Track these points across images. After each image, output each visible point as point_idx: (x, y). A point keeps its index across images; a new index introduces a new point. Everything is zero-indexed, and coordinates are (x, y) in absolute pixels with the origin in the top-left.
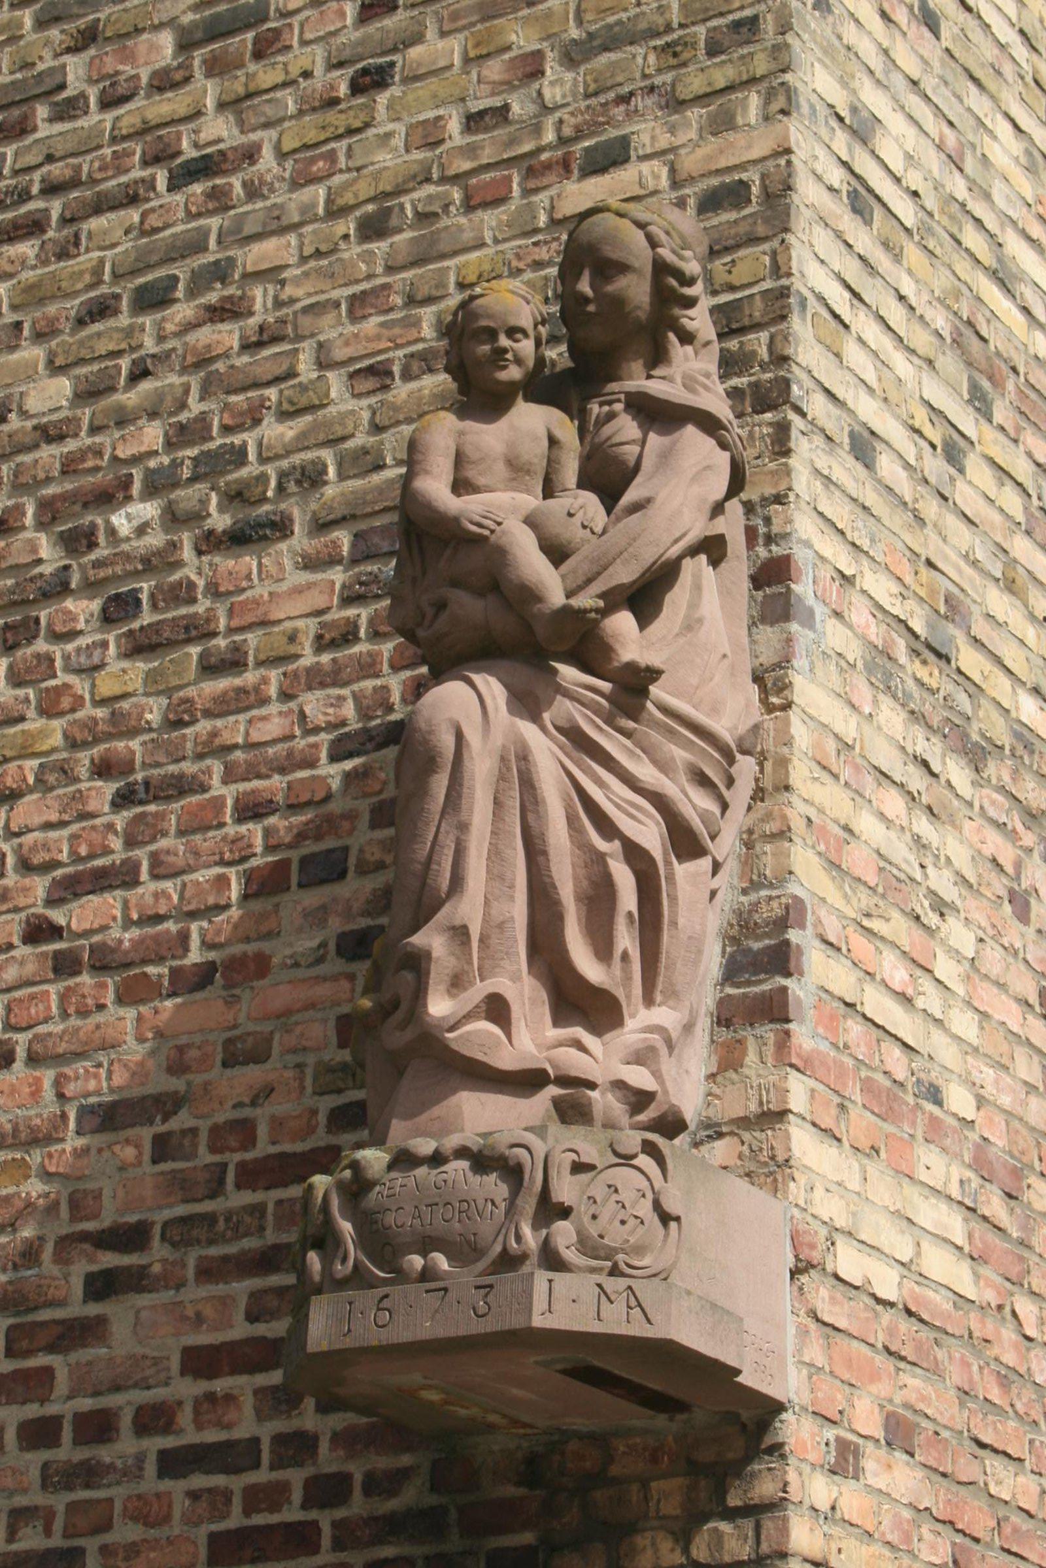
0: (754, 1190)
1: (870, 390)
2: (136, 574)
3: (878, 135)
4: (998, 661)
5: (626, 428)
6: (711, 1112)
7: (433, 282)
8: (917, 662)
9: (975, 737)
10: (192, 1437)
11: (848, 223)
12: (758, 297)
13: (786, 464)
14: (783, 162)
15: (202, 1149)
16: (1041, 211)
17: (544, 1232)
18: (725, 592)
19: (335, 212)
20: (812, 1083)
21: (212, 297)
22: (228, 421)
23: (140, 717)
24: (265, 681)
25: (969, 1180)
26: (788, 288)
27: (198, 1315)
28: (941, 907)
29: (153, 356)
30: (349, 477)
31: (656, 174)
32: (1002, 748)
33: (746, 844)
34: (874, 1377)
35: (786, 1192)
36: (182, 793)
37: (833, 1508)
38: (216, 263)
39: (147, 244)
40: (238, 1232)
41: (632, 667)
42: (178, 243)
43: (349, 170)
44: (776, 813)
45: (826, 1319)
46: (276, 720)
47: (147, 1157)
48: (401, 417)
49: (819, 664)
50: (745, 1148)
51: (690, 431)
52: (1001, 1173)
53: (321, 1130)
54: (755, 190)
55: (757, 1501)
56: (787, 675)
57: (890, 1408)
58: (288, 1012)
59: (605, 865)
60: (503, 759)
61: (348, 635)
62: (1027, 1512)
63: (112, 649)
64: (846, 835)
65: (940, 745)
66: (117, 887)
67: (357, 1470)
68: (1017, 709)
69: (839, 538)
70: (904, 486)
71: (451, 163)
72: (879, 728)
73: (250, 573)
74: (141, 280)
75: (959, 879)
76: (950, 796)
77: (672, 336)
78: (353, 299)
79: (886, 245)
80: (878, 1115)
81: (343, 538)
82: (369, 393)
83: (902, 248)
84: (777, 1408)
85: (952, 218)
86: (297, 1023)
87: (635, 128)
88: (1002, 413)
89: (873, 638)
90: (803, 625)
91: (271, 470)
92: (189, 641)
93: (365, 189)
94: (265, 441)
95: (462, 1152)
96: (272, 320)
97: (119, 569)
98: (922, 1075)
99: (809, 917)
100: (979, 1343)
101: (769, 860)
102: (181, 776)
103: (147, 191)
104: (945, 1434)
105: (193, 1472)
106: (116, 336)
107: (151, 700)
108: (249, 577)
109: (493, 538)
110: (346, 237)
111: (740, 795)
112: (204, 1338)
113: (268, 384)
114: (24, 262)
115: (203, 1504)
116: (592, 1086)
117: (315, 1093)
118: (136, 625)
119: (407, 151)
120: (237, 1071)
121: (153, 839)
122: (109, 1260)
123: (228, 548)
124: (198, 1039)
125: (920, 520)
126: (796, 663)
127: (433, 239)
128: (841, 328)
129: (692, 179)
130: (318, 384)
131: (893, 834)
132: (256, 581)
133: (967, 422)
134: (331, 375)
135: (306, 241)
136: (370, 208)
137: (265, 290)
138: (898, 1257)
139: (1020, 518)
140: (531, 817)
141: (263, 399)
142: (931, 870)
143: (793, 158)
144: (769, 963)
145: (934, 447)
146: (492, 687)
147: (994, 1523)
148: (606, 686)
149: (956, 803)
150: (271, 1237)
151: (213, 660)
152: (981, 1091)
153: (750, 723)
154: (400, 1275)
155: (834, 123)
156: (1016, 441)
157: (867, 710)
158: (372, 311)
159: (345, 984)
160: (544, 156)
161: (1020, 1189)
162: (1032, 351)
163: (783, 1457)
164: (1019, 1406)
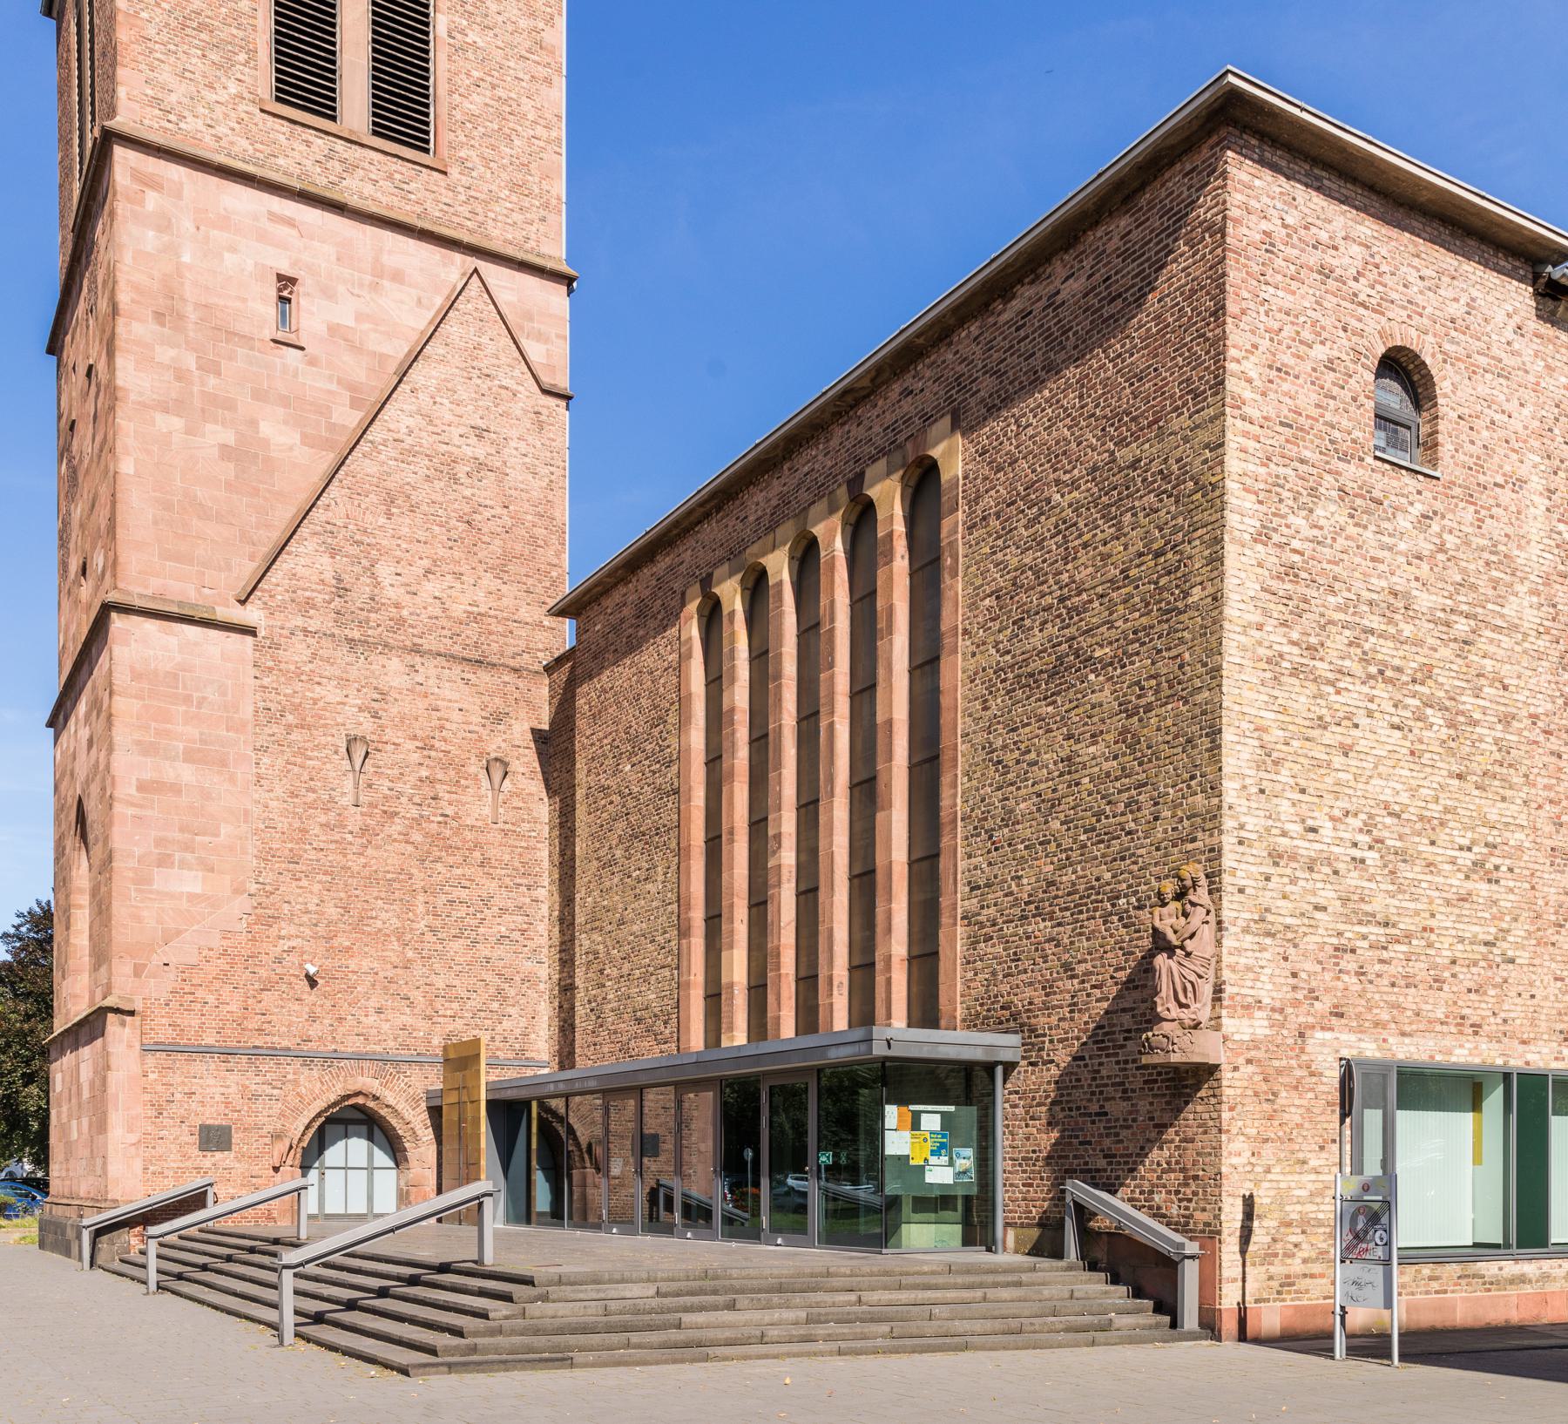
5: (1188, 906)
114: (1214, 733)
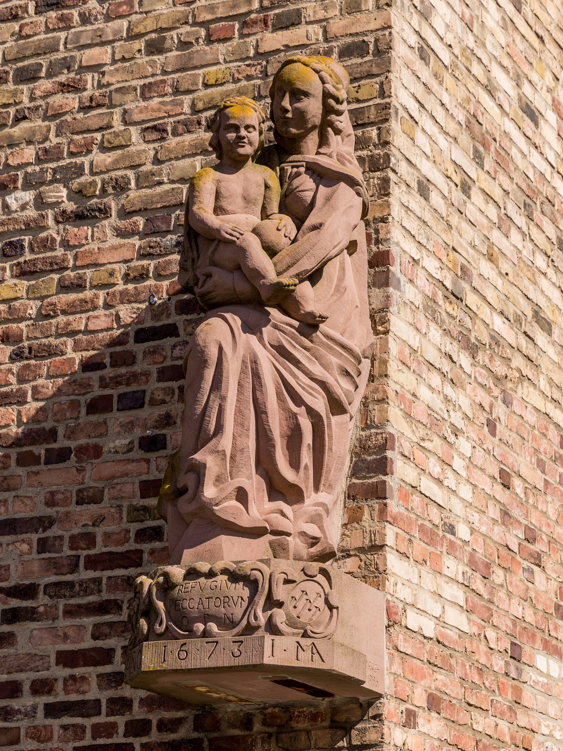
0: (366, 586)
1: (428, 157)
2: (21, 232)
3: (433, 15)
4: (484, 298)
6: (344, 543)
7: (190, 82)
8: (447, 304)
9: (473, 340)
10: (62, 697)
11: (418, 65)
12: (373, 107)
13: (387, 201)
14: (387, 33)
15: (66, 548)
16: (509, 50)
17: (269, 612)
18: (356, 271)
19: (132, 36)
20: (397, 530)
21: (62, 78)
22: (73, 149)
23: (25, 311)
24: (96, 296)
25: (467, 572)
26: (389, 104)
27: (65, 634)
28: (456, 432)
29: (29, 108)
30: (143, 188)
31: (316, 31)
32: (485, 345)
33: (364, 404)
34: (423, 677)
35: (384, 586)
36: (50, 355)
37: (404, 744)
38: (65, 58)
39: (24, 44)
40: (86, 592)
41: (311, 315)
42: (42, 45)
43: (141, 13)
44: (380, 389)
45: (402, 650)
46: (103, 319)
47: (35, 549)
48: (173, 156)
49: (402, 309)
50: (363, 563)
51: (342, 185)
52: (481, 566)
53: (132, 540)
54: (371, 47)
55: (368, 743)
56: (387, 315)
57: (430, 691)
58: (113, 477)
59: (297, 418)
60: (243, 362)
61: (143, 276)
62: (490, 736)
63: (8, 273)
64: (413, 399)
65: (457, 346)
66: (15, 404)
67: (154, 718)
68: (493, 324)
69: (413, 239)
70: (443, 209)
71: (200, 14)
72: (429, 340)
73: (87, 236)
74: (20, 64)
75: (464, 416)
76: (461, 372)
77: (329, 129)
78: (144, 87)
79: (436, 75)
80: (426, 543)
81: (140, 221)
82: (154, 141)
83: (443, 77)
84: (379, 696)
85: (467, 58)
86: (117, 484)
87: (304, 5)
88: (489, 164)
89: (427, 292)
90: (395, 288)
91: (98, 179)
92: (52, 271)
93: (150, 25)
94: (94, 163)
95: (225, 571)
96: (97, 94)
97: (11, 227)
98: (446, 520)
99: (397, 444)
100: (468, 653)
101: (376, 413)
102: (50, 345)
103: (23, 13)
104: (454, 701)
105: (64, 715)
106: (7, 95)
107: (31, 302)
108: (86, 238)
109: (238, 242)
110: (139, 51)
111: (363, 381)
112: (68, 647)
113: (96, 130)
115: (70, 733)
116: (289, 534)
117: (128, 521)
118: (21, 260)
119: (174, 5)
120: (85, 507)
121: (35, 379)
122: (15, 603)
123: (75, 221)
124: (62, 488)
125: (450, 226)
126: (391, 309)
127: (190, 57)
128: (414, 124)
129: (336, 38)
130: (125, 133)
131: (435, 396)
132: (90, 241)
133: (472, 170)
134: (132, 129)
135: (117, 51)
136: (153, 35)
137: (93, 77)
138: (434, 615)
139: (496, 220)
140: (258, 394)
141: (93, 139)
142: (452, 413)
143: (393, 31)
144: (376, 468)
145: (457, 186)
146: (236, 321)
147: (474, 744)
148: (296, 324)
149: (463, 376)
150: (105, 596)
151: (67, 282)
152: (473, 525)
153: (369, 343)
154: (191, 633)
155: (412, 10)
156: (494, 179)
157: (424, 331)
158: (156, 95)
159: (144, 465)
160: (253, 16)
161: (489, 574)
162: (502, 129)
163: (381, 721)
164: (487, 684)
